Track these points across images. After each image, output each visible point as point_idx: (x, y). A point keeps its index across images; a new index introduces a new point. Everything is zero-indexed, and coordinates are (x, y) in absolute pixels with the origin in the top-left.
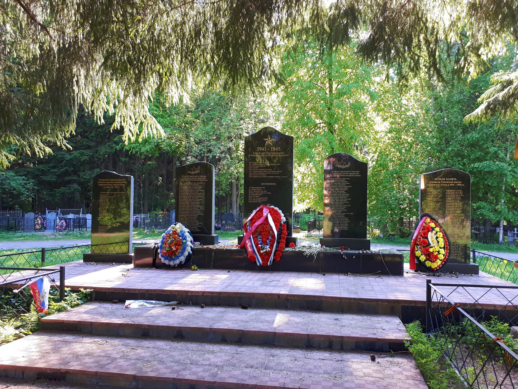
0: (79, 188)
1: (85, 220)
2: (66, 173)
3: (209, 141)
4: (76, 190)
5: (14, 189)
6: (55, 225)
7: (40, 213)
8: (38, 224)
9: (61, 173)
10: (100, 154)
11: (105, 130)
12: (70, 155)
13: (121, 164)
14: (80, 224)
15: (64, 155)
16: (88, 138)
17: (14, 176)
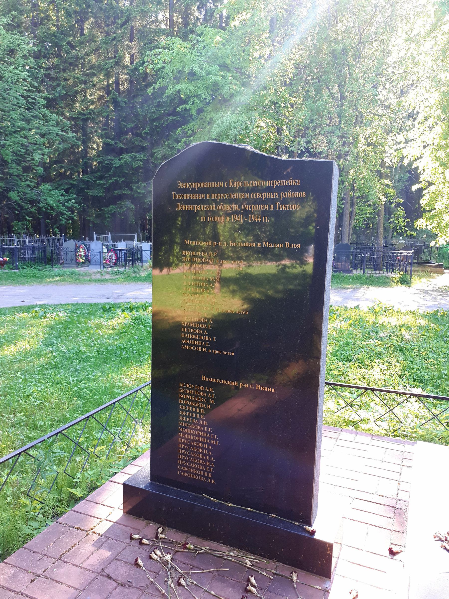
0: (133, 206)
1: (140, 250)
2: (116, 186)
4: (129, 208)
5: (52, 208)
6: (101, 258)
7: (87, 239)
8: (80, 255)
9: (110, 185)
10: (157, 158)
11: (163, 124)
12: (120, 160)
14: (134, 257)
15: (112, 160)
16: (141, 137)
17: (50, 190)
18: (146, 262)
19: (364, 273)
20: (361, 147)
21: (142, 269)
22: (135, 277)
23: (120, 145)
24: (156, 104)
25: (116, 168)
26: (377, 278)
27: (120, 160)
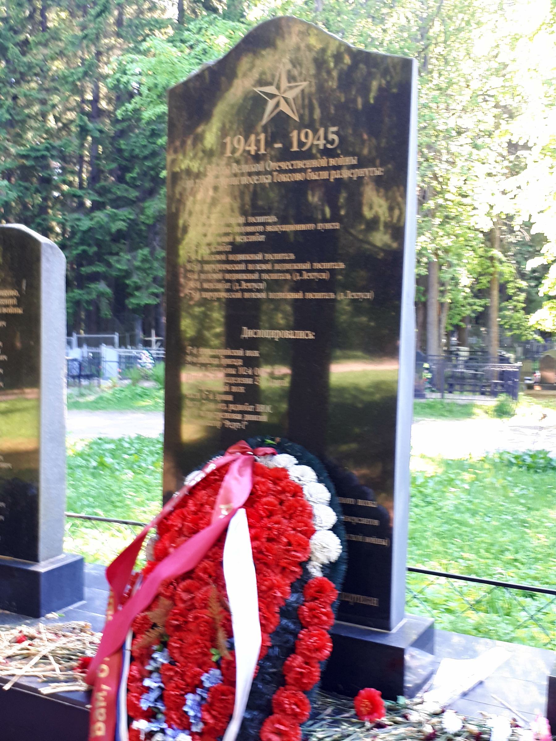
12: (91, 219)
15: (79, 220)
19: (443, 397)
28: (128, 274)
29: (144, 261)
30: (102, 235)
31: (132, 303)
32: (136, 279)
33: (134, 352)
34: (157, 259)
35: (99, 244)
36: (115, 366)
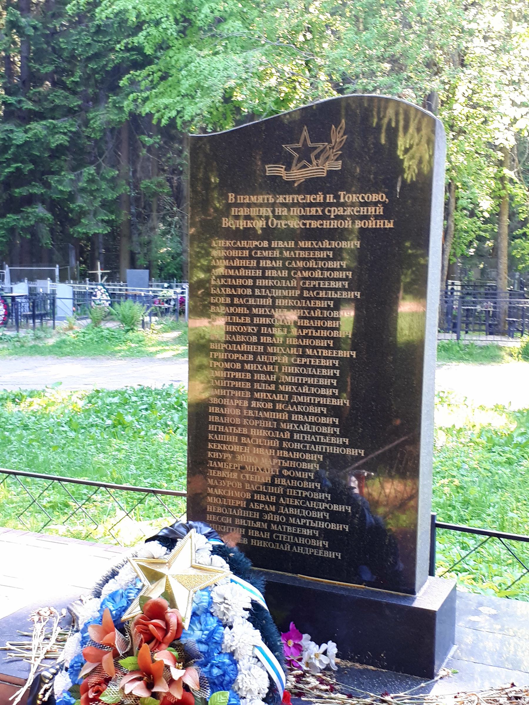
0: (49, 215)
3: (373, 74)
4: (42, 220)
11: (106, 65)
12: (26, 132)
13: (144, 152)
15: (12, 131)
18: (62, 319)
19: (458, 338)
20: (459, 109)
21: (54, 332)
22: (34, 346)
23: (28, 105)
24: (93, 30)
25: (18, 146)
26: (481, 348)
27: (26, 132)
28: (71, 197)
29: (91, 181)
30: (39, 151)
31: (79, 233)
32: (81, 202)
33: (87, 287)
34: (103, 179)
35: (34, 160)
36: (69, 303)
